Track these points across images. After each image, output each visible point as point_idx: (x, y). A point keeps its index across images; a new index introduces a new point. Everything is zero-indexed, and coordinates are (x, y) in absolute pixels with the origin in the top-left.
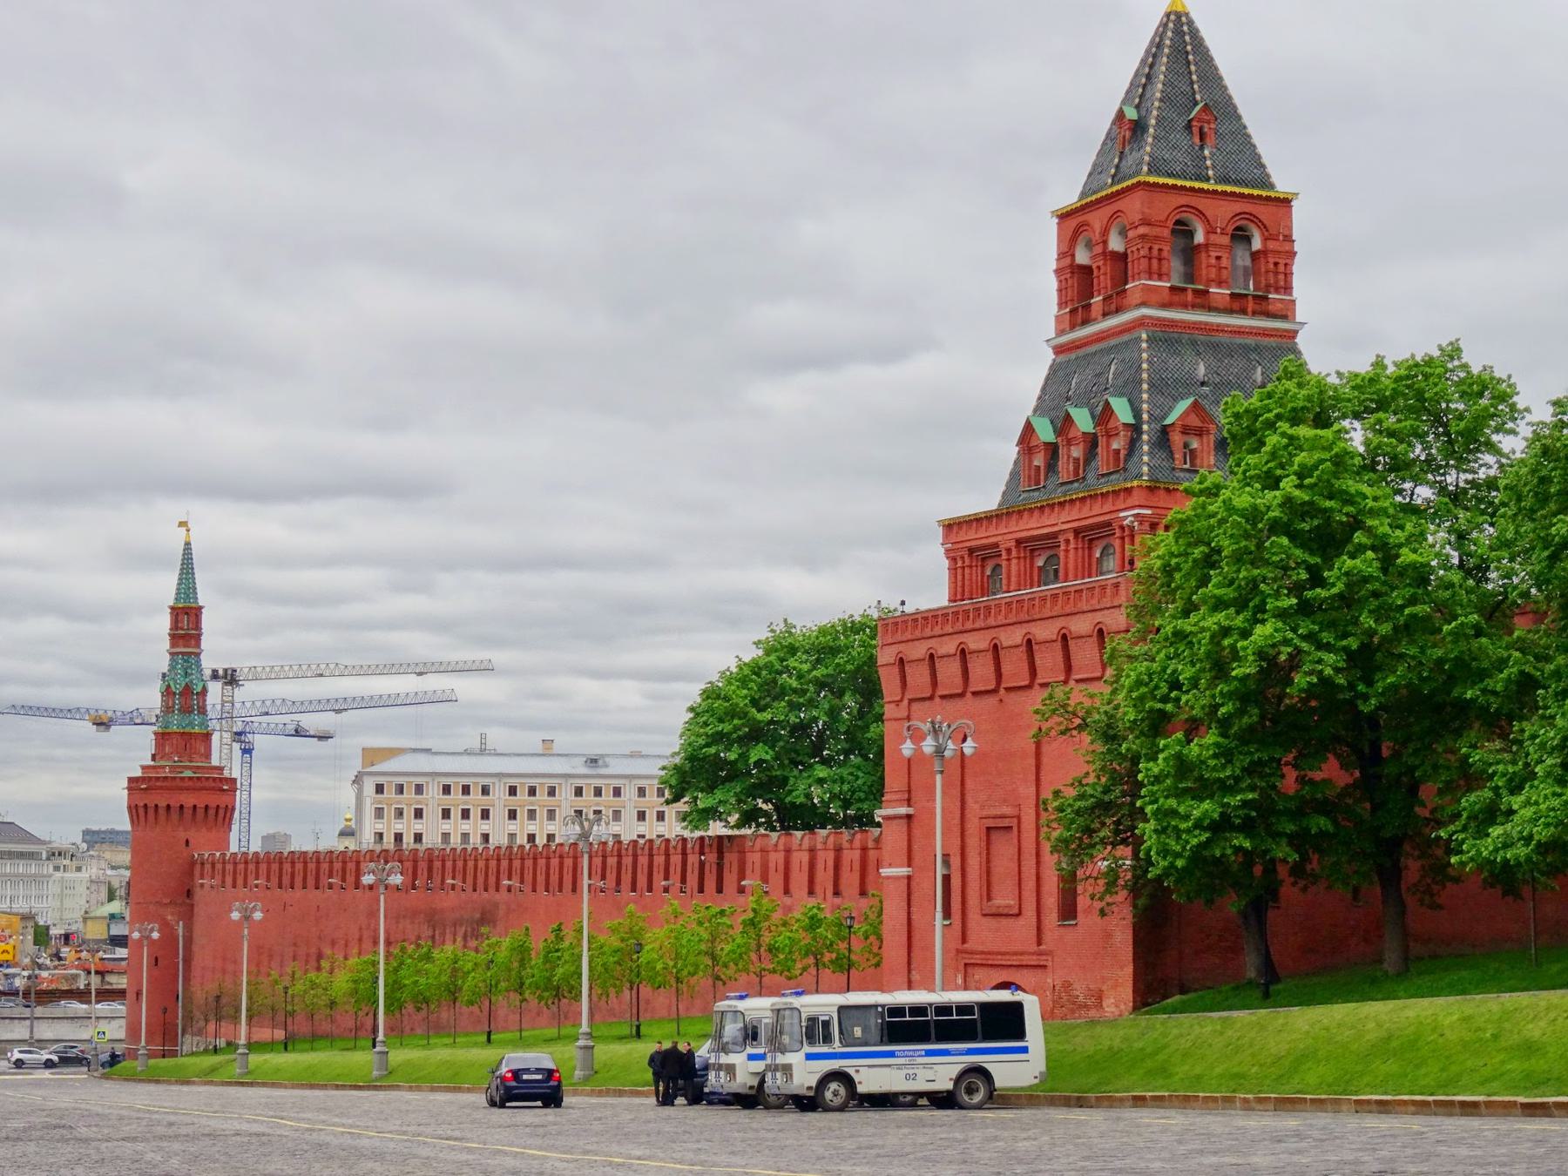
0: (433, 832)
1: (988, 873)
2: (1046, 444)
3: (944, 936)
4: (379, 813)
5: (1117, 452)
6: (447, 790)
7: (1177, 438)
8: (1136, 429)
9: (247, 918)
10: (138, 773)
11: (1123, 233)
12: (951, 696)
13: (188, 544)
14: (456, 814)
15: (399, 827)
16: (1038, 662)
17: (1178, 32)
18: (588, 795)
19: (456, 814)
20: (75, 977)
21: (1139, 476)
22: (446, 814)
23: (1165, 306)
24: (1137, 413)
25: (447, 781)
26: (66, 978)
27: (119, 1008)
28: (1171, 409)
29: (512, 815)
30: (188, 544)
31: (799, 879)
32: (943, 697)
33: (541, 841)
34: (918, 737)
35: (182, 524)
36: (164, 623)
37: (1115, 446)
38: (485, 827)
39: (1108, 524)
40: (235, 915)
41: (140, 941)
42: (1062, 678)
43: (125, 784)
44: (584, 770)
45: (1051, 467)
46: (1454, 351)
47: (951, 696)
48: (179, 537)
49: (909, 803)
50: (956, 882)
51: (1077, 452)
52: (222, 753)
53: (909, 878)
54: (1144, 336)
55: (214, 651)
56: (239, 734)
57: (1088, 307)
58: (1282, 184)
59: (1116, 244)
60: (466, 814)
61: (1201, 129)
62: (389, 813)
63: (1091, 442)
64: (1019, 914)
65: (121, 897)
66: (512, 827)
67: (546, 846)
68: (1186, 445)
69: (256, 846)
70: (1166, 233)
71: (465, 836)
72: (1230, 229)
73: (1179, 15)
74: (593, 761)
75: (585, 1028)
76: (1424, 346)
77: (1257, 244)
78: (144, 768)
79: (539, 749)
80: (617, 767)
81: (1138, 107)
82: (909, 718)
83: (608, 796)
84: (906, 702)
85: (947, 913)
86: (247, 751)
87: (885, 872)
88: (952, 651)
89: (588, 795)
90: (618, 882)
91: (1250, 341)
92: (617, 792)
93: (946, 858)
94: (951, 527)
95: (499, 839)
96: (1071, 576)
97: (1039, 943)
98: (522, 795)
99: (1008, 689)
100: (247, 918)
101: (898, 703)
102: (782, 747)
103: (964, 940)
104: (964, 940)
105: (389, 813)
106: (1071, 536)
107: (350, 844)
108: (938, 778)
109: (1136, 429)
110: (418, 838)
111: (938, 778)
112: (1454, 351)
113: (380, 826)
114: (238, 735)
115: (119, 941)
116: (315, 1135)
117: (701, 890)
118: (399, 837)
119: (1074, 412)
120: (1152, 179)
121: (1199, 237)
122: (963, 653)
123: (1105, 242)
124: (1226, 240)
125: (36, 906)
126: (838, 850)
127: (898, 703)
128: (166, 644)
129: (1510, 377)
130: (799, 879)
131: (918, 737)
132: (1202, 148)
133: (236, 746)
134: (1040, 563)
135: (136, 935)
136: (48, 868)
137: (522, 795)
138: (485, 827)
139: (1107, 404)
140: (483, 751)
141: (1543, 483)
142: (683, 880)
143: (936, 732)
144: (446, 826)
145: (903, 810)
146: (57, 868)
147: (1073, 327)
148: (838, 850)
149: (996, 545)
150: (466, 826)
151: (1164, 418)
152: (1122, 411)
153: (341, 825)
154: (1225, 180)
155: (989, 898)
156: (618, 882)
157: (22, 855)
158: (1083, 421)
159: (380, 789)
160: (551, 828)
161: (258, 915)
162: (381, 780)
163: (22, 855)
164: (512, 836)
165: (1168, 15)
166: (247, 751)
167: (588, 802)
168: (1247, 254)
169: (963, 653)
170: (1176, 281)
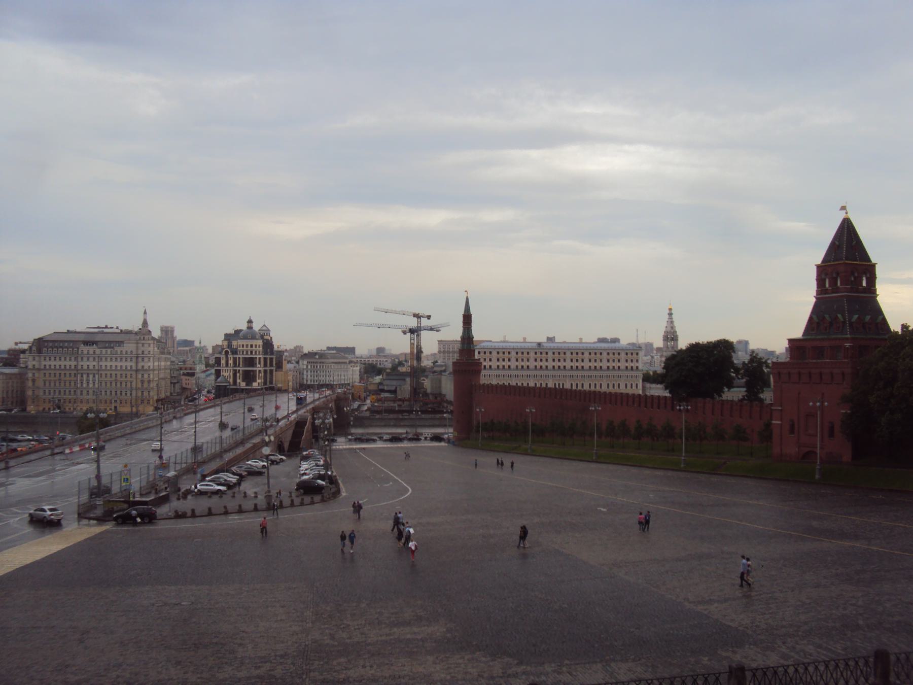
6: (498, 353)
8: (844, 322)
13: (467, 298)
17: (848, 227)
23: (850, 292)
24: (844, 319)
30: (467, 298)
34: (680, 406)
46: (814, 296)
48: (465, 295)
49: (781, 406)
53: (781, 424)
54: (845, 300)
60: (504, 360)
79: (522, 340)
92: (547, 353)
96: (268, 371)
102: (599, 407)
109: (844, 322)
112: (814, 296)
122: (789, 373)
131: (680, 406)
139: (837, 316)
141: (39, 351)
145: (780, 408)
146: (351, 366)
154: (861, 261)
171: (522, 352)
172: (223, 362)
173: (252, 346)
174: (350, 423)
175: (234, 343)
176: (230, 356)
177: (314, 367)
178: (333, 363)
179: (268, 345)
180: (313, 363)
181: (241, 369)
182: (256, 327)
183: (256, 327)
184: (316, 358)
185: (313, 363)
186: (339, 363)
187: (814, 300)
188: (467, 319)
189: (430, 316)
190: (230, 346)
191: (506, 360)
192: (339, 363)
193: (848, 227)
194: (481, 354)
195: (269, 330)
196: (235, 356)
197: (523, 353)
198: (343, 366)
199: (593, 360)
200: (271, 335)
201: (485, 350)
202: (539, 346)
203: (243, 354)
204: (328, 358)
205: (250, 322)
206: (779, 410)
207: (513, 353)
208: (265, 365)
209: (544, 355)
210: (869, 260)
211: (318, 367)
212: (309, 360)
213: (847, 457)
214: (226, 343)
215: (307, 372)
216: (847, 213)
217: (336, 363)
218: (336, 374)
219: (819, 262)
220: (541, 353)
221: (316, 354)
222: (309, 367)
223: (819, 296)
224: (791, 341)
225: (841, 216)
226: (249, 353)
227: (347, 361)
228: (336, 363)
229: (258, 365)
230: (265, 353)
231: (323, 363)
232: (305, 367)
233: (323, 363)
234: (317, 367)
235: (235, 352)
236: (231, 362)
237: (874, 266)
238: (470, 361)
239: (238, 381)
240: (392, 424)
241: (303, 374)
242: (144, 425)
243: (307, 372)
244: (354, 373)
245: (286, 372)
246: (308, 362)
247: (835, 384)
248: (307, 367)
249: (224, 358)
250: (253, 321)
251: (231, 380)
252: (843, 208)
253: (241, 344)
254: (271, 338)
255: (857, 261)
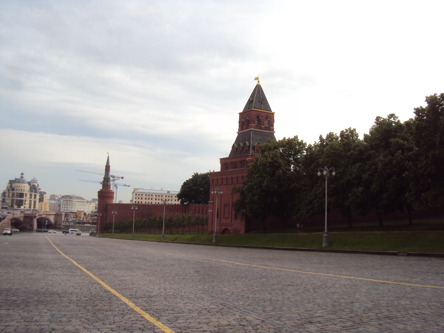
0: (144, 201)
1: (224, 212)
2: (236, 148)
3: (217, 221)
4: (136, 198)
5: (246, 149)
7: (256, 148)
9: (114, 213)
10: (99, 190)
11: (249, 117)
12: (225, 185)
13: (108, 156)
14: (147, 199)
15: (139, 200)
16: (233, 180)
17: (259, 88)
18: (167, 197)
19: (147, 199)
20: (89, 221)
21: (250, 153)
22: (146, 199)
24: (250, 144)
25: (146, 194)
26: (88, 221)
27: (95, 226)
28: (255, 144)
29: (156, 199)
30: (108, 156)
31: (197, 211)
32: (219, 185)
33: (157, 203)
34: (214, 191)
35: (108, 153)
36: (104, 168)
37: (246, 149)
38: (152, 201)
39: (245, 160)
40: (113, 213)
41: (99, 216)
42: (226, 184)
43: (97, 192)
44: (167, 193)
45: (237, 151)
47: (225, 185)
50: (219, 213)
51: (241, 149)
52: (112, 188)
53: (213, 212)
55: (111, 173)
56: (115, 185)
57: (243, 128)
58: (273, 111)
59: (248, 118)
60: (149, 199)
61: (261, 102)
62: (137, 198)
63: (243, 148)
64: (229, 218)
65: (63, 273)
66: (156, 201)
67: (158, 204)
68: (257, 149)
69: (117, 202)
70: (255, 117)
71: (149, 202)
72: (265, 117)
73: (259, 85)
74: (168, 192)
75: (163, 232)
76: (292, 137)
77: (269, 120)
78: (100, 190)
79: (160, 190)
80: (171, 193)
81: (252, 98)
82: (214, 188)
83: (170, 197)
84: (213, 186)
85: (218, 217)
86: (117, 188)
87: (209, 211)
88: (220, 178)
89: (167, 197)
90: (170, 210)
91: (267, 134)
92: (172, 197)
93: (218, 209)
94: (221, 160)
95: (154, 203)
97: (231, 222)
98: (157, 196)
99: (229, 184)
100: (114, 213)
101: (212, 186)
103: (220, 221)
104: (220, 221)
105: (137, 198)
106: (239, 162)
107: (131, 203)
108: (217, 197)
109: (249, 146)
110: (141, 202)
111: (217, 197)
113: (136, 200)
114: (115, 185)
115: (96, 216)
116: (155, 307)
117: (182, 212)
118: (139, 202)
119: (246, 142)
120: (253, 109)
121: (260, 118)
122: (222, 179)
123: (246, 118)
124: (264, 119)
125: (84, 210)
126: (203, 207)
127: (212, 186)
128: (104, 171)
129: (333, 132)
130: (197, 211)
131: (214, 191)
132: (261, 105)
133: (115, 187)
134: (234, 166)
135: (98, 215)
136: (86, 204)
137: (157, 196)
138: (152, 201)
139: (245, 142)
140: (152, 190)
142: (180, 211)
143: (217, 191)
144: (146, 201)
145: (212, 202)
146: (88, 204)
147: (241, 131)
148: (203, 207)
149: (228, 163)
150: (149, 201)
151: (254, 144)
152: (247, 143)
153: (130, 200)
155: (224, 215)
156: (170, 210)
157: (82, 202)
158: (242, 144)
159: (136, 194)
160: (159, 201)
161: (116, 213)
162: (136, 193)
163: (82, 202)
164: (156, 203)
165: (257, 85)
166: (117, 188)
167: (167, 198)
168: (267, 121)
169: (222, 179)
170: (257, 124)
171: (158, 195)
172: (7, 195)
173: (19, 187)
174: (45, 224)
175: (14, 185)
176: (11, 192)
177: (66, 203)
178: (77, 201)
179: (34, 188)
180: (66, 201)
181: (15, 199)
182: (28, 178)
183: (28, 178)
184: (68, 199)
185: (66, 201)
186: (81, 202)
187: (237, 135)
188: (108, 168)
189: (123, 177)
190: (11, 186)
191: (150, 199)
192: (81, 202)
193: (259, 88)
194: (137, 196)
195: (37, 180)
196: (13, 192)
197: (159, 196)
198: (82, 203)
199: (157, 199)
200: (38, 183)
201: (139, 193)
202: (168, 193)
203: (17, 191)
204: (74, 199)
205: (22, 174)
206: (211, 203)
207: (154, 196)
208: (31, 197)
209: (170, 197)
210: (270, 111)
211: (69, 203)
212: (64, 199)
213: (242, 231)
214: (9, 185)
215: (63, 205)
216: (259, 82)
217: (79, 202)
218: (76, 207)
219: (241, 111)
220: (169, 196)
221: (68, 196)
222: (64, 203)
223: (239, 132)
224: (222, 160)
225: (256, 83)
226: (20, 190)
227: (86, 201)
228: (79, 202)
229: (25, 197)
230: (31, 190)
231: (72, 201)
232: (62, 203)
233: (72, 201)
234: (68, 203)
235: (13, 190)
236: (11, 195)
237: (273, 114)
238: (107, 191)
239: (14, 205)
240: (85, 229)
241: (60, 206)
242: (422, 316)
243: (63, 205)
244: (89, 208)
245: (45, 204)
246: (63, 200)
247: (239, 184)
248: (63, 202)
249: (8, 193)
250: (24, 173)
251: (10, 205)
252: (257, 79)
253: (16, 185)
254: (38, 185)
255: (262, 110)
